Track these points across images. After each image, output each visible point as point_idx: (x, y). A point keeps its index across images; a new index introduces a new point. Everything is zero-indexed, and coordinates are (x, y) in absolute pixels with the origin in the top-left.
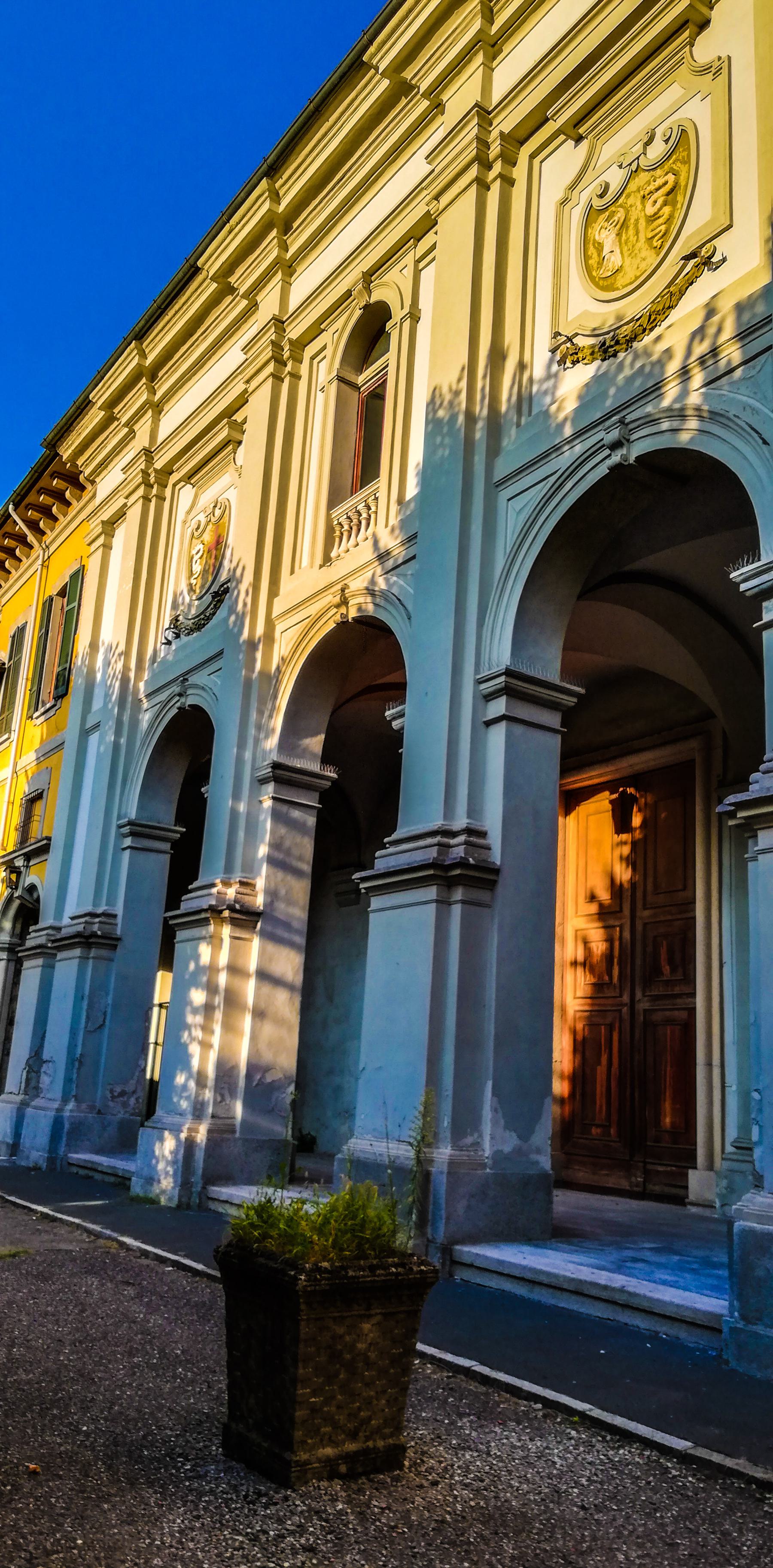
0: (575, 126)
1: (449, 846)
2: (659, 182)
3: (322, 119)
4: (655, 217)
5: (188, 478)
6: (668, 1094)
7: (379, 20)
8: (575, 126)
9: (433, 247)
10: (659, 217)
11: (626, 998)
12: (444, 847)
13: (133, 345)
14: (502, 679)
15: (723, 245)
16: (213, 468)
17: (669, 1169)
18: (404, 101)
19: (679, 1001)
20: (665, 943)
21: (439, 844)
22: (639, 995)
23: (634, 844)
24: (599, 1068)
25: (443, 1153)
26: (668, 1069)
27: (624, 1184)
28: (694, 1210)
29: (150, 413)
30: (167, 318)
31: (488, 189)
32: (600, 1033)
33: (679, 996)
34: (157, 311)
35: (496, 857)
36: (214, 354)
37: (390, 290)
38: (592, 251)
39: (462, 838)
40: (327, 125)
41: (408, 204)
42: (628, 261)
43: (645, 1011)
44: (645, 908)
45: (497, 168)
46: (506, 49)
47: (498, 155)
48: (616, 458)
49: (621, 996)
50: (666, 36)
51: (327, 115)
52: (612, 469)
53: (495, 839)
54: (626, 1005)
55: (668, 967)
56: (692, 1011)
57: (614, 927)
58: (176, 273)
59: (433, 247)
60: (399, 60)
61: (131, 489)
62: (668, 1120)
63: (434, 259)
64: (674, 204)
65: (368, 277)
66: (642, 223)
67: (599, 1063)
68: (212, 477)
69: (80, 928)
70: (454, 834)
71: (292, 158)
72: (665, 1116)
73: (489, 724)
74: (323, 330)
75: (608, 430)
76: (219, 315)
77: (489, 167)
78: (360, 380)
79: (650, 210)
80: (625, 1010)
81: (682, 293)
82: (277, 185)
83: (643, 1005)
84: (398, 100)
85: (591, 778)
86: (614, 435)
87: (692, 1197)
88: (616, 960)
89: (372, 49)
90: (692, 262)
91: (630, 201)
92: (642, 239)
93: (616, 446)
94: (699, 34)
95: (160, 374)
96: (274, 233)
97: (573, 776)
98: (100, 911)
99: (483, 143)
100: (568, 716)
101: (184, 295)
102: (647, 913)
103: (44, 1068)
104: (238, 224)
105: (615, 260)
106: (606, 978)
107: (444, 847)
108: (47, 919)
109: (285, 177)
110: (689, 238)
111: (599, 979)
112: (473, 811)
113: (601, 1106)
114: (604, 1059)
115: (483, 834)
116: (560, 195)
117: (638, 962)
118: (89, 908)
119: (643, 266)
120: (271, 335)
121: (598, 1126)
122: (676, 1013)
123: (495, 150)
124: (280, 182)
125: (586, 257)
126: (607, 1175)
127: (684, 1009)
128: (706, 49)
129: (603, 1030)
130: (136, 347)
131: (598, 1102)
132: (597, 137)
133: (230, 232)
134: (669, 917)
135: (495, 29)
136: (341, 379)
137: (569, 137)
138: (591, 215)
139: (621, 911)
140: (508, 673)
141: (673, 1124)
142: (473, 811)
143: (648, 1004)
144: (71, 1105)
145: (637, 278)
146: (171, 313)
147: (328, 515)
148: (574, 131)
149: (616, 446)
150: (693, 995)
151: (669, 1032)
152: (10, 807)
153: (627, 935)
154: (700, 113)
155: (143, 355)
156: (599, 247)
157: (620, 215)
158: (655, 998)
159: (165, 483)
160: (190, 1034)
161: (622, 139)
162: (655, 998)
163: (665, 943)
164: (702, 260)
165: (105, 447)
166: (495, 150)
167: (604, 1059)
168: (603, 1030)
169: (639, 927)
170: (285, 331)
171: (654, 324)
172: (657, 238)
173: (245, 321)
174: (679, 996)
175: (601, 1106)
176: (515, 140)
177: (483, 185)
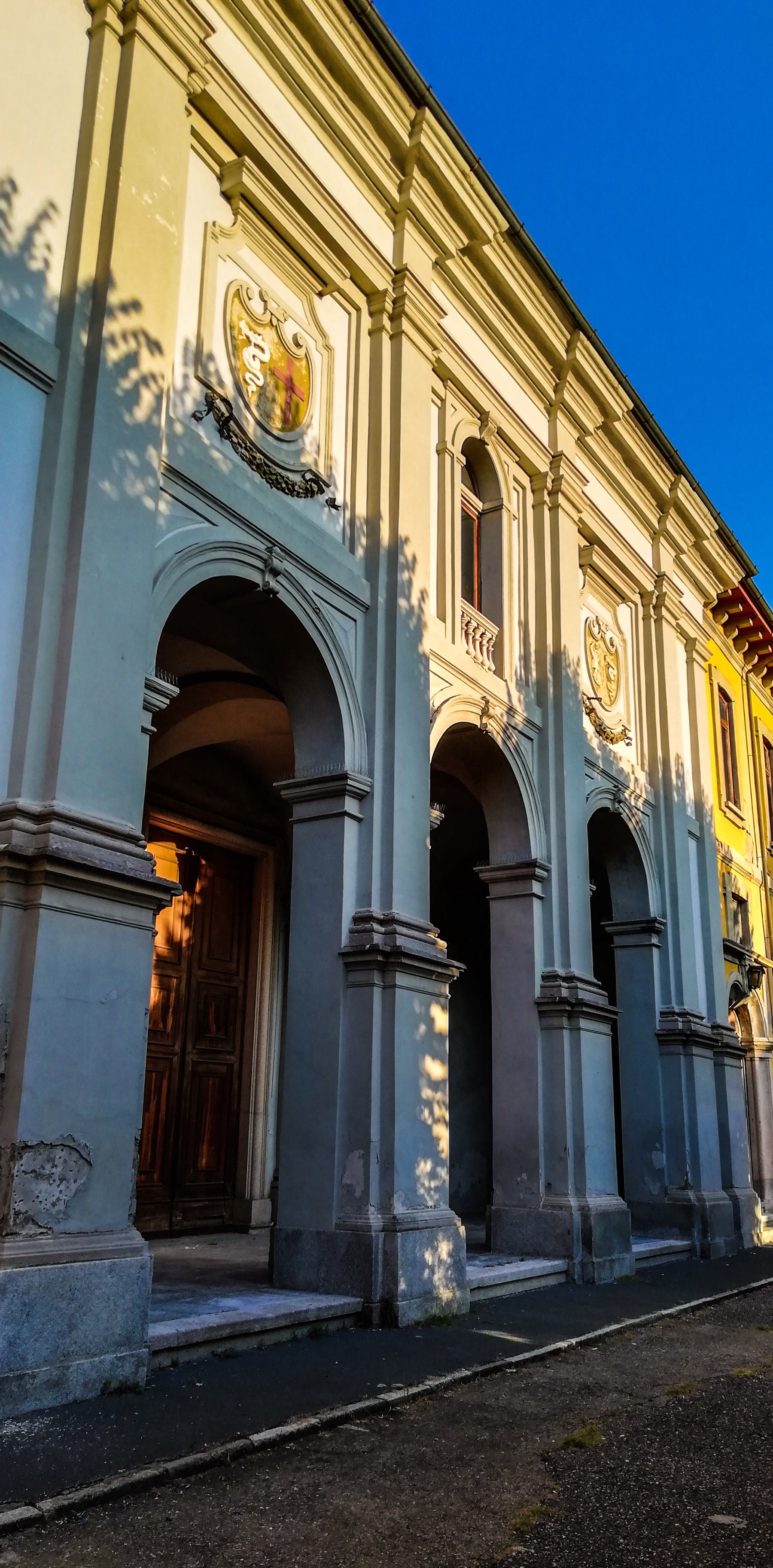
0: (243, 196)
3: (545, 290)
7: (401, 54)
8: (243, 196)
11: (177, 1048)
17: (202, 1204)
18: (549, 367)
19: (220, 1056)
22: (189, 1048)
23: (193, 907)
26: (208, 1115)
33: (221, 1052)
34: (643, 416)
36: (321, 126)
41: (511, 416)
43: (193, 1062)
44: (200, 969)
49: (173, 1046)
50: (321, 275)
51: (547, 294)
54: (177, 1054)
55: (214, 1026)
57: (170, 977)
58: (585, 313)
60: (581, 371)
61: (672, 610)
62: (204, 1161)
71: (520, 256)
76: (368, 138)
80: (175, 1059)
84: (550, 363)
85: (169, 823)
87: (253, 1223)
88: (171, 1010)
96: (466, 241)
97: (176, 819)
101: (343, 8)
104: (472, 186)
106: (161, 1025)
109: (505, 245)
111: (154, 1025)
122: (218, 1067)
127: (225, 1064)
133: (463, 173)
134: (217, 982)
139: (180, 964)
141: (206, 1163)
143: (197, 1056)
146: (353, 28)
158: (202, 1052)
160: (432, 1113)
162: (202, 1052)
169: (193, 979)
173: (371, 189)
174: (221, 1052)
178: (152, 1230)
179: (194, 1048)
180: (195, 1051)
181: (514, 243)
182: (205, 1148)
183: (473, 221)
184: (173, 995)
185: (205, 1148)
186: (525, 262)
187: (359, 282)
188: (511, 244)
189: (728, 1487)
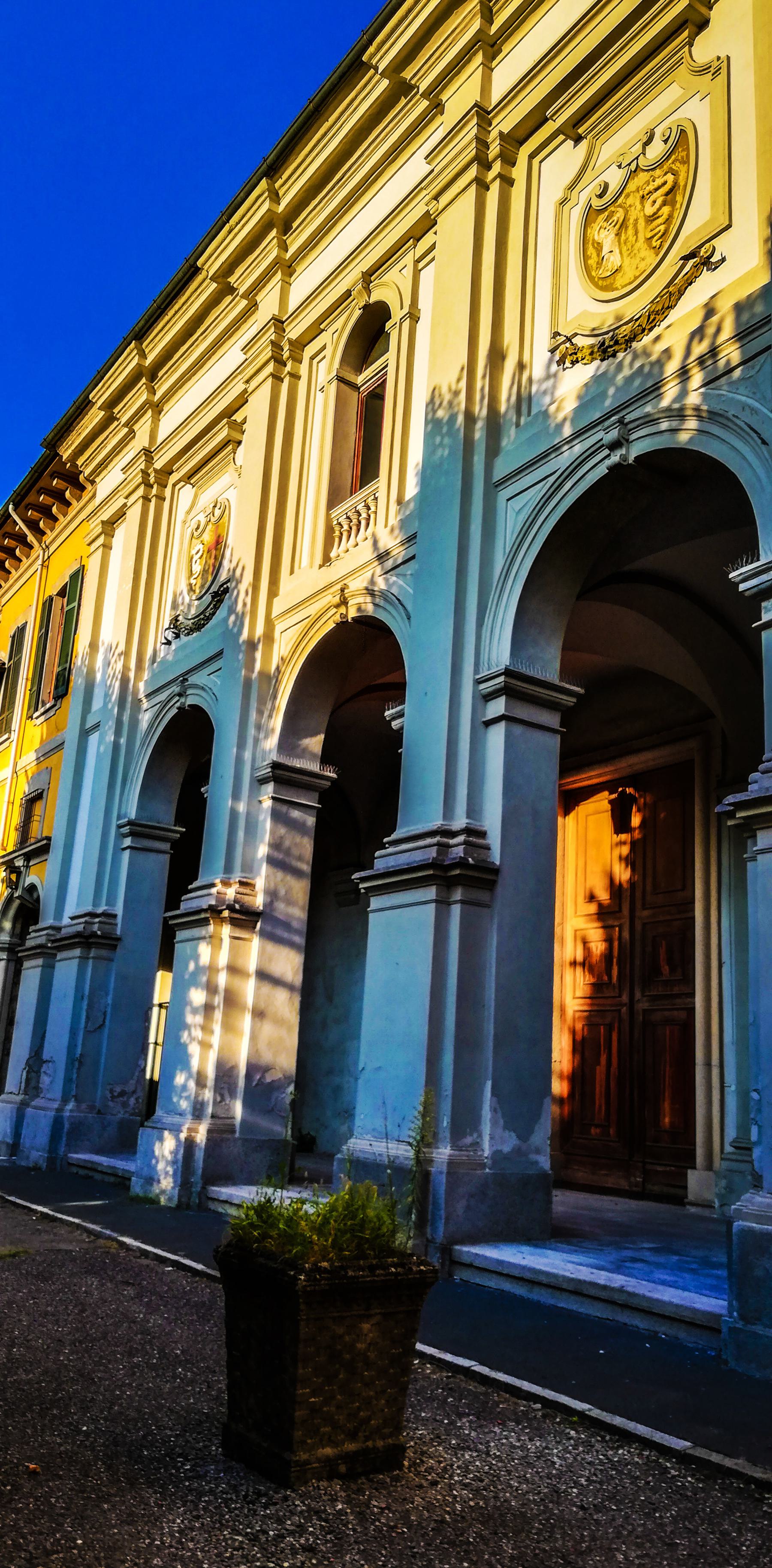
0: (574, 126)
1: (449, 846)
2: (658, 182)
4: (654, 217)
5: (188, 478)
6: (667, 1094)
8: (574, 126)
9: (433, 247)
10: (658, 217)
11: (625, 998)
12: (443, 848)
13: (133, 345)
14: (502, 679)
15: (722, 245)
16: (213, 468)
18: (403, 101)
19: (678, 1001)
20: (664, 942)
21: (438, 844)
22: (638, 995)
23: (633, 844)
24: (598, 1067)
25: (443, 1153)
26: (668, 1069)
27: (624, 1184)
28: (693, 1210)
29: (149, 413)
30: (167, 318)
31: (488, 189)
32: (599, 1033)
35: (496, 856)
36: (213, 354)
37: (389, 290)
38: (591, 251)
39: (461, 838)
40: (327, 125)
41: (407, 204)
42: (627, 261)
43: (644, 1011)
44: (644, 908)
45: (497, 168)
46: (506, 49)
47: (497, 154)
48: (615, 458)
49: (620, 996)
52: (611, 469)
53: (495, 839)
54: (625, 1005)
55: (667, 968)
56: (692, 1010)
58: (175, 273)
59: (433, 247)
62: (667, 1120)
63: (433, 259)
64: (673, 203)
65: (368, 277)
66: (642, 223)
67: (599, 1063)
68: (211, 478)
69: (80, 928)
70: (453, 834)
72: (664, 1101)
73: (488, 724)
74: (323, 330)
75: (607, 430)
76: (219, 315)
77: (489, 167)
78: (360, 380)
79: (649, 210)
81: (681, 293)
82: (277, 185)
83: (643, 1005)
84: (398, 100)
85: (590, 778)
86: (614, 434)
87: (691, 1197)
88: (615, 960)
89: (371, 49)
90: (691, 262)
91: (629, 201)
92: (641, 239)
93: (614, 446)
94: (698, 34)
95: (160, 374)
98: (100, 911)
99: (482, 143)
100: (568, 715)
102: (646, 913)
103: (44, 1068)
104: (237, 224)
105: (614, 260)
106: (606, 978)
107: (443, 848)
108: (47, 920)
109: (285, 177)
110: (688, 238)
111: (598, 978)
112: (474, 809)
113: (600, 1106)
114: (603, 1059)
115: (483, 834)
116: (559, 195)
117: (638, 962)
118: (89, 908)
119: (642, 266)
120: (271, 334)
121: (597, 1126)
123: (494, 150)
124: (280, 182)
125: (585, 257)
126: (606, 1175)
128: (705, 49)
129: (602, 1031)
130: (136, 347)
131: (597, 1102)
132: (596, 137)
133: (230, 232)
135: (494, 29)
136: (341, 379)
137: (568, 137)
138: (590, 215)
139: (620, 911)
140: (507, 672)
141: (671, 1123)
142: (473, 810)
144: (71, 1106)
145: (636, 278)
147: (328, 515)
148: (573, 131)
149: (614, 446)
150: (692, 995)
151: (668, 1032)
152: (10, 807)
153: (626, 935)
154: (699, 113)
155: (143, 355)
156: (599, 247)
157: (619, 215)
159: (165, 483)
161: (621, 139)
162: (654, 999)
163: (664, 942)
164: (702, 260)
165: (105, 446)
166: (494, 150)
167: (603, 1059)
168: (602, 1031)
169: (638, 927)
170: (284, 331)
171: (653, 324)
172: (656, 238)
175: (600, 1106)
176: (514, 140)
177: (482, 185)
178: (609, 1185)
179: (643, 996)
180: (645, 999)
181: (282, 165)
182: (667, 1106)
183: (256, 229)
184: (616, 944)
185: (667, 1106)
186: (297, 149)
187: (237, 406)
188: (282, 170)
189: (187, 1501)
